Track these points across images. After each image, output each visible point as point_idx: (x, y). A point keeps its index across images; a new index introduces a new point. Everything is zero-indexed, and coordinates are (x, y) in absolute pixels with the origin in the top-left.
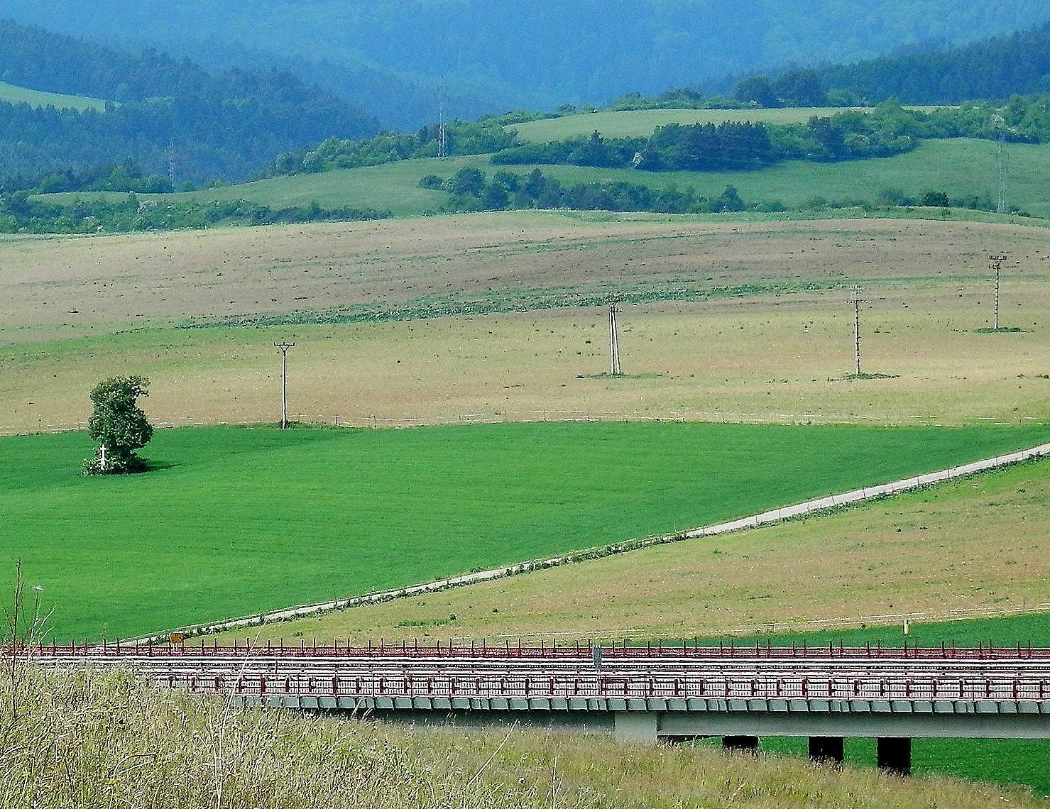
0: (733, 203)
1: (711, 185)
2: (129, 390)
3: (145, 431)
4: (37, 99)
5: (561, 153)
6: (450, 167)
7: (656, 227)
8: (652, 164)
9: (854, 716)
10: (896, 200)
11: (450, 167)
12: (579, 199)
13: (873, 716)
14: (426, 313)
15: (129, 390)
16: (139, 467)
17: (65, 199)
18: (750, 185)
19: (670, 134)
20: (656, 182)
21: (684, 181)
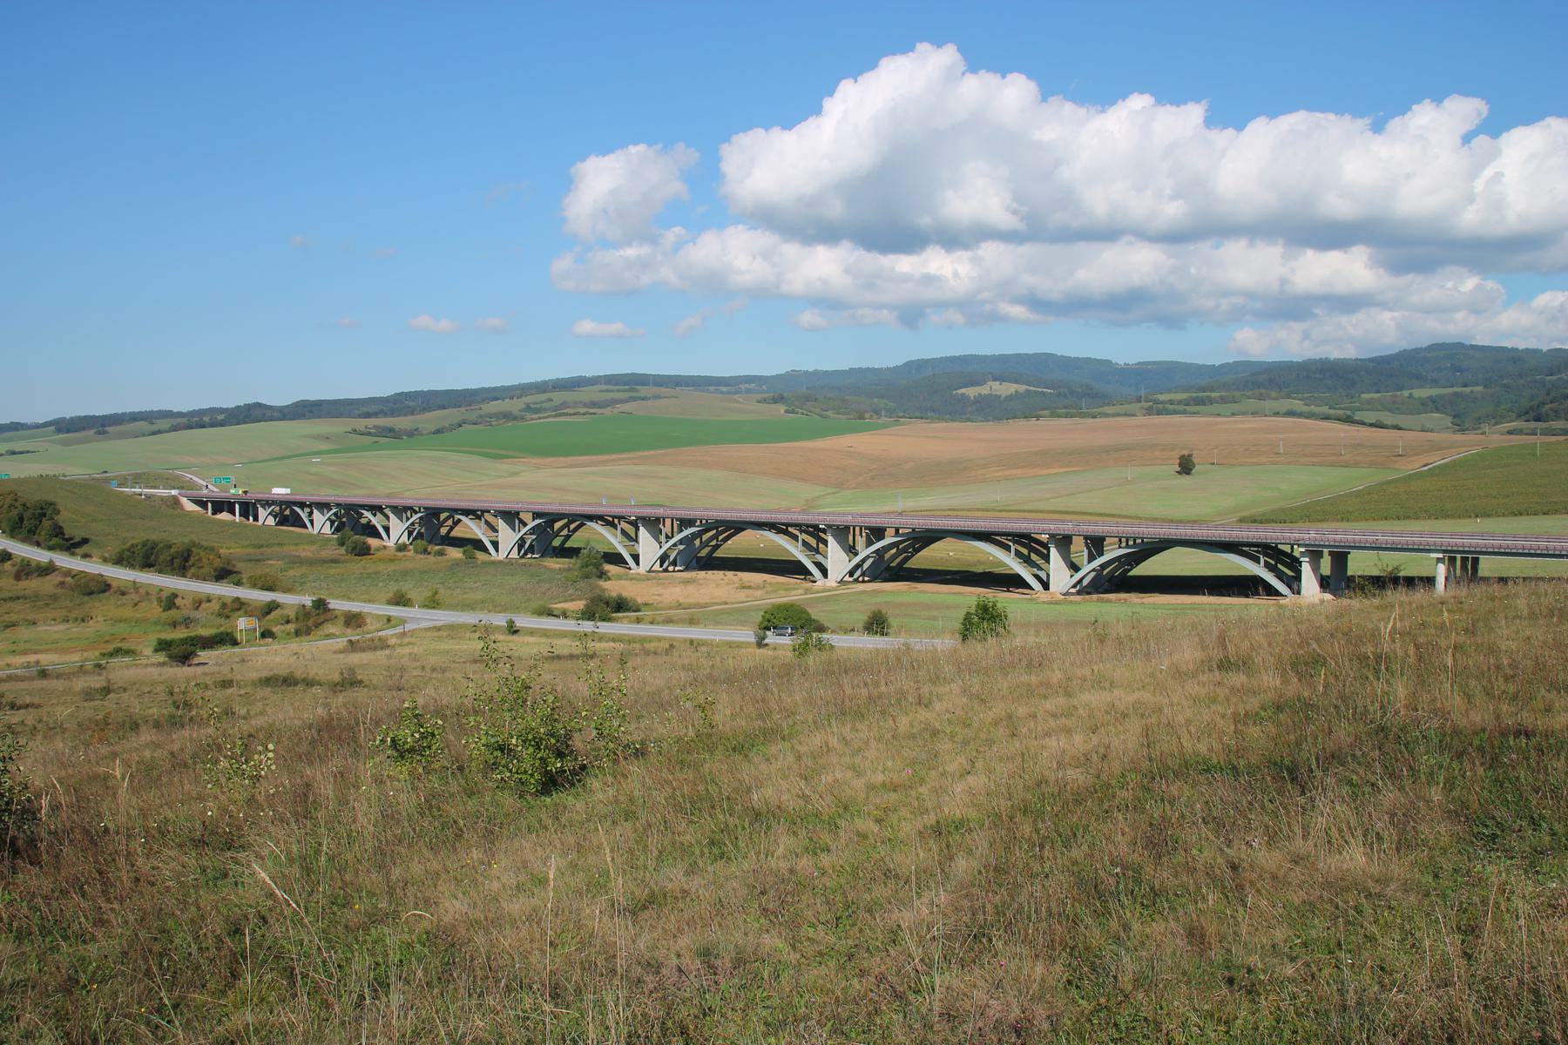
4: (1040, 390)
12: (1175, 412)
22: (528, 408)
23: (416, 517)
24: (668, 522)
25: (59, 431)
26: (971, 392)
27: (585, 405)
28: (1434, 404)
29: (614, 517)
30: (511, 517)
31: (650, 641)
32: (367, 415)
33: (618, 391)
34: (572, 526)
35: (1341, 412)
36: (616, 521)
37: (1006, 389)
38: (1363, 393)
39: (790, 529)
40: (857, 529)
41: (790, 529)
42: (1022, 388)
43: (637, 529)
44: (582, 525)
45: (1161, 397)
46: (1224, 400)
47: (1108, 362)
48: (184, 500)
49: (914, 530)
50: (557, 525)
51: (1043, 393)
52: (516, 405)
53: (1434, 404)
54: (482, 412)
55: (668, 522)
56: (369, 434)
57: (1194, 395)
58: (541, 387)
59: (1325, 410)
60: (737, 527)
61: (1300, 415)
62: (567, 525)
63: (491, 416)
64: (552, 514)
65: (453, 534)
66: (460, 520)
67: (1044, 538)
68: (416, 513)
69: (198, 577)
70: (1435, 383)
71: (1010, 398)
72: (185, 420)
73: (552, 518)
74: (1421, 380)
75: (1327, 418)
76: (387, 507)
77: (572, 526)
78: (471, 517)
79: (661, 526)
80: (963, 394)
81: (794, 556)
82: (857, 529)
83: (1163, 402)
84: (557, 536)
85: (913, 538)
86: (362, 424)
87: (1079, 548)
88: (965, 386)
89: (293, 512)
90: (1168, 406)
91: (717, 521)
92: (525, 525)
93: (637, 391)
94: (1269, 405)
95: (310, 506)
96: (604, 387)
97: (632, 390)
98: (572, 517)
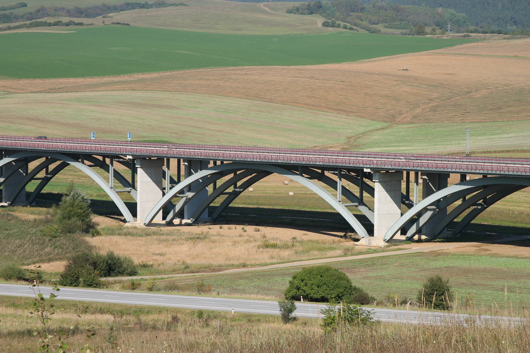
24: (173, 163)
29: (105, 156)
34: (52, 167)
39: (327, 173)
40: (412, 175)
44: (64, 165)
49: (485, 176)
50: (32, 165)
77: (52, 167)
82: (412, 175)
84: (32, 178)
85: (484, 187)
91: (235, 163)
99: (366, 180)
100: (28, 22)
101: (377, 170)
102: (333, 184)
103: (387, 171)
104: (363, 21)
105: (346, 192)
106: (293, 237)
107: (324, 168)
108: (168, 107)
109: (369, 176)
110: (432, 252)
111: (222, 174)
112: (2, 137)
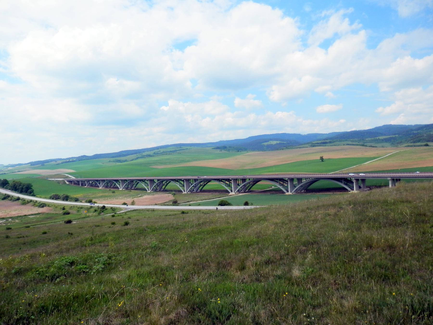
0: (325, 146)
1: (324, 145)
2: (322, 157)
3: (323, 159)
4: (283, 142)
5: (316, 143)
6: (310, 144)
7: (251, 153)
8: (321, 144)
9: (359, 178)
10: (335, 145)
11: (310, 144)
12: (317, 146)
13: (361, 178)
14: (325, 152)
15: (322, 157)
16: (323, 161)
17: (289, 147)
18: (327, 145)
19: (321, 142)
20: (321, 145)
21: (322, 145)
22: (154, 153)
23: (127, 182)
24: (192, 180)
25: (31, 165)
26: (266, 144)
27: (169, 152)
28: (386, 140)
29: (178, 180)
30: (152, 181)
31: (144, 152)
32: (113, 157)
33: (177, 148)
34: (167, 182)
35: (361, 144)
36: (179, 181)
37: (274, 142)
38: (366, 138)
39: (222, 180)
40: (239, 180)
41: (222, 180)
42: (278, 142)
43: (184, 182)
44: (170, 182)
45: (314, 142)
46: (330, 142)
47: (300, 135)
48: (66, 181)
49: (253, 179)
50: (164, 182)
51: (284, 143)
52: (151, 153)
53: (386, 140)
54: (143, 155)
55: (192, 180)
56: (114, 162)
57: (322, 141)
58: (158, 148)
59: (357, 143)
60: (209, 181)
61: (351, 145)
62: (166, 182)
63: (144, 156)
64: (162, 180)
65: (166, 188)
66: (139, 182)
67: (287, 179)
68: (127, 181)
69: (70, 201)
70: (385, 135)
71: (275, 145)
72: (65, 161)
73: (162, 181)
74: (382, 134)
75: (358, 145)
76: (120, 180)
77: (167, 182)
78: (141, 181)
79: (190, 181)
80: (263, 144)
81: (341, 186)
82: (239, 180)
83: (314, 144)
84: (164, 185)
85: (254, 181)
86: (112, 159)
87: (295, 182)
88: (264, 142)
89: (95, 183)
90: (315, 144)
91: (204, 179)
92: (155, 183)
93: (182, 148)
94: (343, 143)
95: (99, 181)
96: (174, 147)
97: (180, 147)
98: (167, 180)
99: (230, 181)
100: (177, 147)
101: (232, 179)
102: (277, 182)
103: (234, 179)
104: (410, 256)
105: (280, 183)
106: (43, 232)
107: (222, 179)
108: (403, 202)
109: (231, 180)
110: (416, 143)
111: (201, 182)
112: (1, 165)
